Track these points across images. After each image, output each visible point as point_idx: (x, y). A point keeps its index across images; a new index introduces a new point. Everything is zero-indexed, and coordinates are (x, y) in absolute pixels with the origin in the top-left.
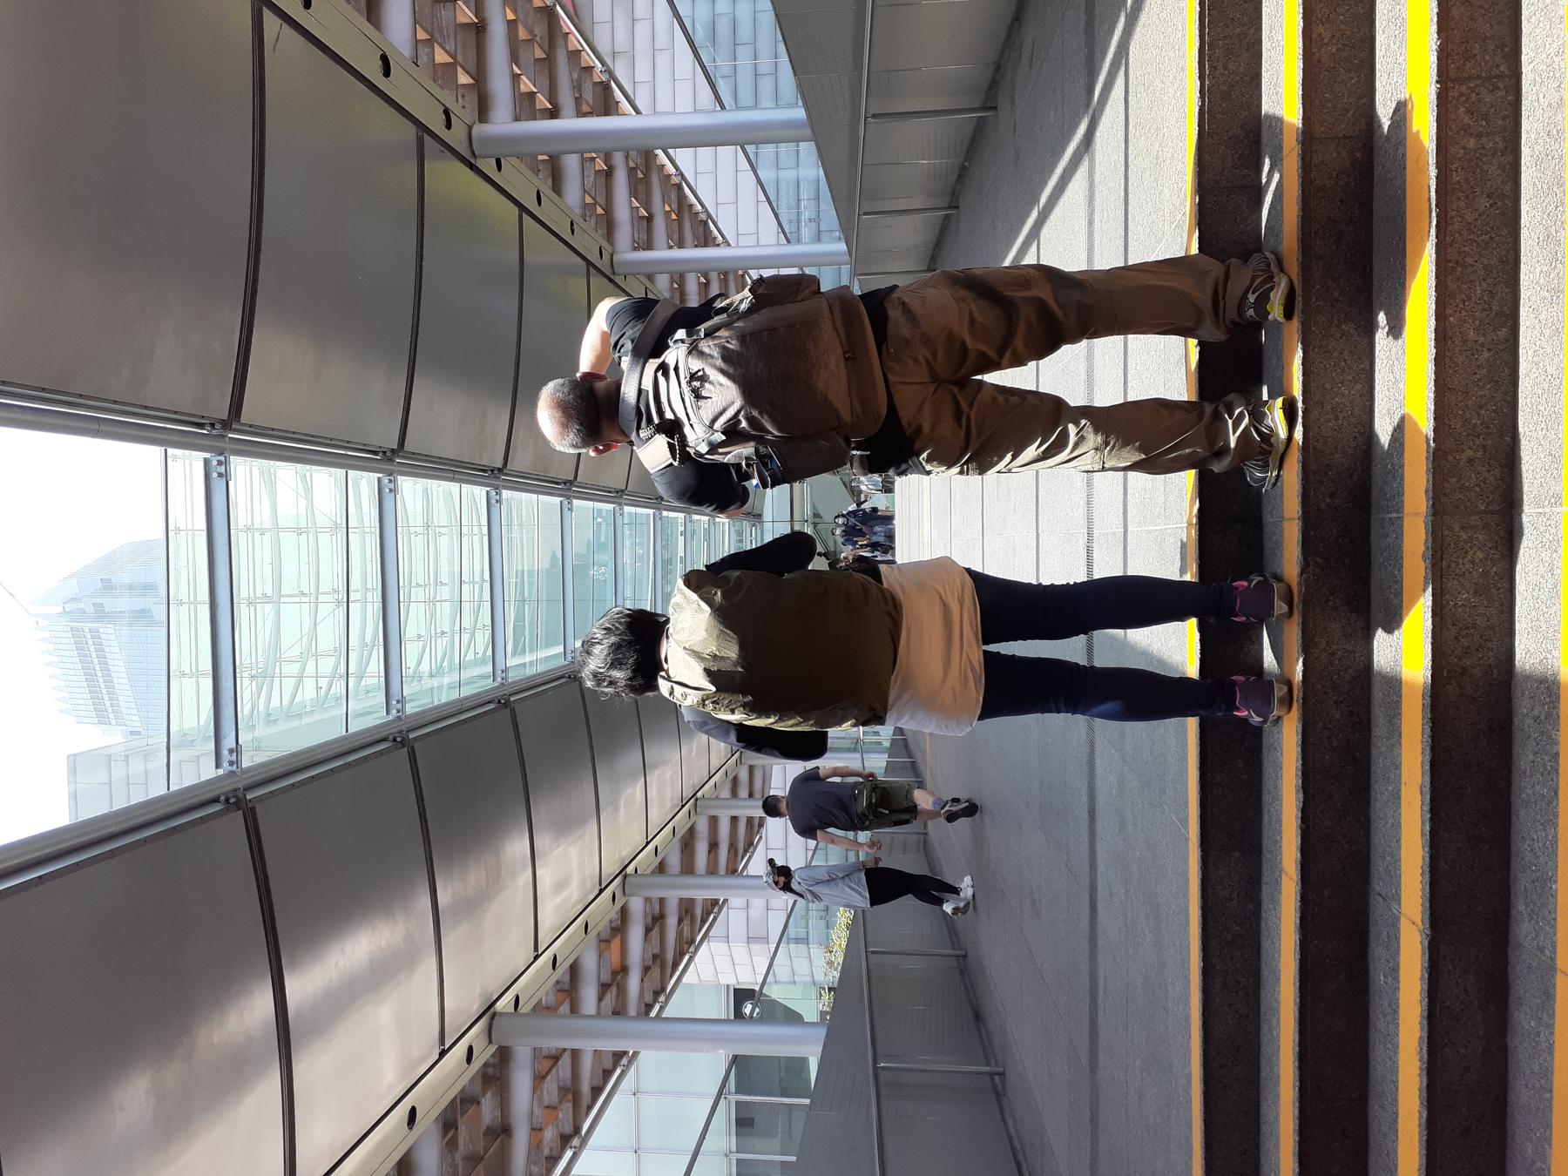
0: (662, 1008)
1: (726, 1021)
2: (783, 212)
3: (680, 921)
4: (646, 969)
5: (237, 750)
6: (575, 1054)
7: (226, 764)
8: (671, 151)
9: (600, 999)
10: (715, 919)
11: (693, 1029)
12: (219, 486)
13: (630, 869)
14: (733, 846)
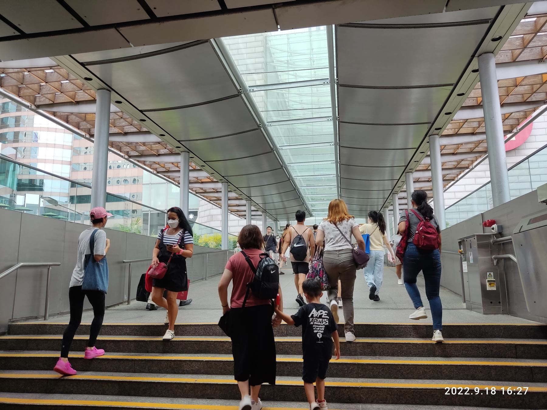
0: (191, 193)
3: (216, 197)
5: (253, 91)
6: (179, 171)
7: (250, 89)
8: (487, 159)
9: (169, 163)
10: (122, 157)
11: (186, 200)
12: (322, 82)
13: (229, 184)
14: (238, 211)
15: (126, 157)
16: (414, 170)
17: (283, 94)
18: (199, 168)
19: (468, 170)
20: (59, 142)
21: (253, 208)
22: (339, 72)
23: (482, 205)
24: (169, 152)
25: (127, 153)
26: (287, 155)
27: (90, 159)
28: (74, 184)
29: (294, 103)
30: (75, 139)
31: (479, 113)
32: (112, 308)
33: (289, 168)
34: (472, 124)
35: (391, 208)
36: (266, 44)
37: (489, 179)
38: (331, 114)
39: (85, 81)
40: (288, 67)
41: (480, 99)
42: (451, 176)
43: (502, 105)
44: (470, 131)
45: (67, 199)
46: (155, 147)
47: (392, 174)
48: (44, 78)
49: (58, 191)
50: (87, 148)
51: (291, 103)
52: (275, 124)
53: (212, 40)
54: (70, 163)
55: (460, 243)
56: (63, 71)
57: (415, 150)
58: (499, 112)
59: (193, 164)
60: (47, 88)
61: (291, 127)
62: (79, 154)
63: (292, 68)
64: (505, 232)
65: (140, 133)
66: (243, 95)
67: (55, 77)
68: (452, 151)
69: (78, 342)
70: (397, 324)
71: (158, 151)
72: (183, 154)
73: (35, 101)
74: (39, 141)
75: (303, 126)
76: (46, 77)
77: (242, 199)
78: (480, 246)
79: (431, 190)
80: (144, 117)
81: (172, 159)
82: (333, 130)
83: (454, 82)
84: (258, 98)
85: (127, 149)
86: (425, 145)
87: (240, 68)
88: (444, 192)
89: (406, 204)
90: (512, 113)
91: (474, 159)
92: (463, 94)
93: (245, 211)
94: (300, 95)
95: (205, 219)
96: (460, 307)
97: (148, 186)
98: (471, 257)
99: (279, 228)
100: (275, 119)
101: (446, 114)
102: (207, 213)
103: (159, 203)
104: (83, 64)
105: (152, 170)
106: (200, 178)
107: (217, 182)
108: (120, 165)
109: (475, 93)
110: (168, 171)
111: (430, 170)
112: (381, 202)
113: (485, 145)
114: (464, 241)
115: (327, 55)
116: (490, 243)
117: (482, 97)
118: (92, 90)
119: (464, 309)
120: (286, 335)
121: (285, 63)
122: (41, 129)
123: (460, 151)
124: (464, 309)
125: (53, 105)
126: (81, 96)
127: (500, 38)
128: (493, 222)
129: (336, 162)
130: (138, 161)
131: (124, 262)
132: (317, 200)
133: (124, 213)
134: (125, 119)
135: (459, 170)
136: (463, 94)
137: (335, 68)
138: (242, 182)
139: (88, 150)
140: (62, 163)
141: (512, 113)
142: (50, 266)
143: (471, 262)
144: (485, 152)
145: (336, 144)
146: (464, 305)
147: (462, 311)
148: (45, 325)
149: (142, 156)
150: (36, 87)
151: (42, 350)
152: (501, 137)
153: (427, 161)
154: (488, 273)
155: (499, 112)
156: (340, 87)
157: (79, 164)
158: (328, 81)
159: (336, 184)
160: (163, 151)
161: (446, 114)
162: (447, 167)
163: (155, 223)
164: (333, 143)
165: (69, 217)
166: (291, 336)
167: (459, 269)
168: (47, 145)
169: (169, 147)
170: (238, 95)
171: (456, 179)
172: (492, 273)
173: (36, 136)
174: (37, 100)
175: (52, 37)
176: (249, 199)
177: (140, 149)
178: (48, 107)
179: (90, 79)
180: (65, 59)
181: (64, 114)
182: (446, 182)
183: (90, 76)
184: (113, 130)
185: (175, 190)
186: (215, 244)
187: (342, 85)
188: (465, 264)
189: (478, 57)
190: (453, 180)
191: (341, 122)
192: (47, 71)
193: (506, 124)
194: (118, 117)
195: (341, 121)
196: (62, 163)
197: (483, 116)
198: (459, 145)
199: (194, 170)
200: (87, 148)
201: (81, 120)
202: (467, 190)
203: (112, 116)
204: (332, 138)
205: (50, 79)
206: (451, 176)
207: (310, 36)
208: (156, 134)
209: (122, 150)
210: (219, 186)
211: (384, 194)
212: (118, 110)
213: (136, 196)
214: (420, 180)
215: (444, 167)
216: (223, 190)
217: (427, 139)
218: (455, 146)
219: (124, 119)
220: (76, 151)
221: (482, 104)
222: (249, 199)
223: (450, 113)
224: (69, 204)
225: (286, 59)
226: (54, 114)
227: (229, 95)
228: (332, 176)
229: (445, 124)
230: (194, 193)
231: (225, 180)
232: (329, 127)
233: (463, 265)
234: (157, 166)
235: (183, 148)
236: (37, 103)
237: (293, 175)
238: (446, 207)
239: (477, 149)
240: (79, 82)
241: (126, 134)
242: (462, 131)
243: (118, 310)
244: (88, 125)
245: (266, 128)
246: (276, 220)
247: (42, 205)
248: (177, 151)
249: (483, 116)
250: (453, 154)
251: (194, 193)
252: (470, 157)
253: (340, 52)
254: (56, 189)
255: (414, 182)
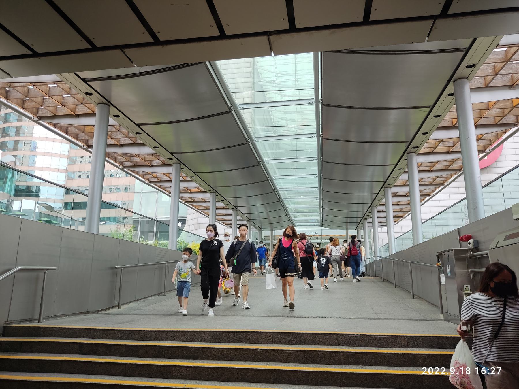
1: (178, 217)
2: (432, 221)
3: (204, 206)
4: (191, 198)
5: (243, 108)
6: (170, 181)
7: (240, 106)
9: (161, 173)
10: (117, 167)
11: (175, 210)
12: (307, 102)
13: (217, 194)
14: (225, 220)
15: (121, 167)
16: (392, 185)
17: (269, 112)
18: (189, 179)
19: (443, 186)
20: (56, 151)
21: (239, 218)
22: (324, 92)
23: (457, 221)
24: (161, 163)
25: (122, 163)
26: (273, 168)
27: (88, 168)
28: (68, 191)
29: (279, 120)
30: (71, 148)
31: (454, 134)
32: (103, 312)
33: (274, 180)
34: (447, 143)
35: (370, 220)
36: (255, 65)
37: (465, 196)
38: (315, 131)
39: (86, 96)
40: (276, 90)
41: (455, 121)
42: (427, 191)
43: (476, 127)
44: (445, 150)
45: (61, 205)
46: (148, 158)
47: (371, 188)
48: (47, 92)
49: (53, 197)
50: (82, 157)
51: (276, 120)
52: (262, 139)
53: (207, 63)
54: (66, 171)
55: (438, 257)
56: (66, 86)
57: (394, 166)
58: (473, 133)
59: (184, 175)
60: (50, 102)
61: (275, 142)
62: (75, 163)
63: (278, 87)
64: (481, 247)
65: (135, 144)
66: (233, 112)
67: (58, 91)
68: (428, 168)
69: (71, 345)
70: (380, 334)
71: (151, 162)
72: (175, 165)
73: (38, 113)
74: (37, 150)
75: (288, 142)
76: (49, 91)
77: (228, 209)
78: (457, 259)
79: (409, 204)
80: (139, 131)
81: (164, 170)
82: (316, 145)
83: (431, 104)
84: (246, 115)
85: (122, 159)
86: (403, 163)
87: (231, 86)
88: (421, 205)
89: (385, 217)
90: (484, 134)
91: (449, 176)
92: (439, 116)
93: (231, 220)
94: (285, 112)
95: (192, 227)
96: (437, 318)
97: (139, 195)
98: (449, 270)
99: (263, 237)
100: (262, 134)
101: (423, 134)
102: (195, 221)
103: (150, 211)
104: (85, 80)
105: (144, 180)
106: (190, 188)
107: (206, 192)
108: (114, 174)
109: (451, 115)
110: (160, 181)
111: (408, 185)
112: (360, 214)
113: (460, 163)
114: (441, 254)
115: (313, 76)
116: (467, 257)
117: (458, 118)
118: (92, 104)
119: (442, 320)
120: (272, 343)
121: (272, 83)
122: (39, 138)
123: (435, 168)
124: (442, 320)
125: (54, 117)
126: (82, 109)
127: (474, 65)
128: (469, 238)
129: (319, 176)
130: (132, 171)
131: (116, 268)
132: (299, 212)
133: (115, 220)
134: (122, 132)
135: (434, 187)
136: (439, 116)
137: (320, 90)
138: (229, 193)
139: (83, 160)
140: (59, 171)
141: (484, 134)
142: (46, 270)
143: (449, 274)
144: (460, 170)
145: (319, 160)
146: (442, 316)
147: (440, 322)
148: (39, 327)
149: (135, 166)
150: (39, 100)
151: (35, 352)
152: (476, 156)
153: (405, 177)
154: (465, 286)
155: (473, 133)
156: (324, 107)
157: (74, 172)
158: (313, 101)
159: (318, 197)
160: (155, 162)
161: (423, 134)
162: (423, 183)
163: (146, 230)
164: (316, 158)
165: (63, 223)
166: (277, 344)
167: (437, 281)
168: (45, 154)
169: (162, 158)
170: (229, 111)
171: (432, 195)
172: (469, 286)
173: (35, 146)
174: (40, 112)
175: (61, 56)
176: (235, 208)
177: (134, 160)
178: (49, 119)
179: (91, 94)
180: (70, 76)
181: (64, 126)
182: (422, 197)
183: (91, 91)
184: (110, 142)
185: (165, 198)
186: (290, 281)
187: (326, 105)
188: (443, 277)
189: (454, 82)
190: (429, 195)
191: (325, 139)
192: (50, 86)
193: (479, 144)
194: (115, 130)
195: (324, 138)
196: (59, 171)
197: (459, 136)
198: (434, 163)
199: (185, 180)
200: (82, 157)
201: (80, 132)
202: (442, 205)
203: (110, 128)
204: (315, 154)
205: (53, 93)
206: (427, 191)
207: (296, 59)
208: (150, 146)
209: (117, 161)
210: (208, 196)
211: (363, 207)
212: (116, 123)
213: (127, 204)
214: (397, 195)
215: (421, 183)
216: (211, 200)
217: (405, 157)
218: (431, 164)
219: (120, 131)
220: (71, 160)
221: (457, 125)
222: (235, 208)
223: (427, 133)
224: (63, 210)
225: (273, 79)
226: (55, 125)
227: (221, 112)
228: (314, 189)
229: (422, 143)
230: (183, 202)
231: (214, 190)
232: (313, 143)
233: (441, 278)
234: (150, 176)
235: (175, 160)
236: (40, 115)
237: (278, 187)
238: (423, 221)
239: (452, 167)
240: (80, 96)
241: (122, 145)
242: (438, 150)
243: (108, 314)
244: (86, 136)
245: (254, 143)
246: (260, 229)
247: (37, 211)
248: (169, 162)
249: (459, 136)
250: (429, 171)
251: (183, 202)
252: (445, 174)
253: (326, 76)
254: (52, 196)
255: (392, 196)
